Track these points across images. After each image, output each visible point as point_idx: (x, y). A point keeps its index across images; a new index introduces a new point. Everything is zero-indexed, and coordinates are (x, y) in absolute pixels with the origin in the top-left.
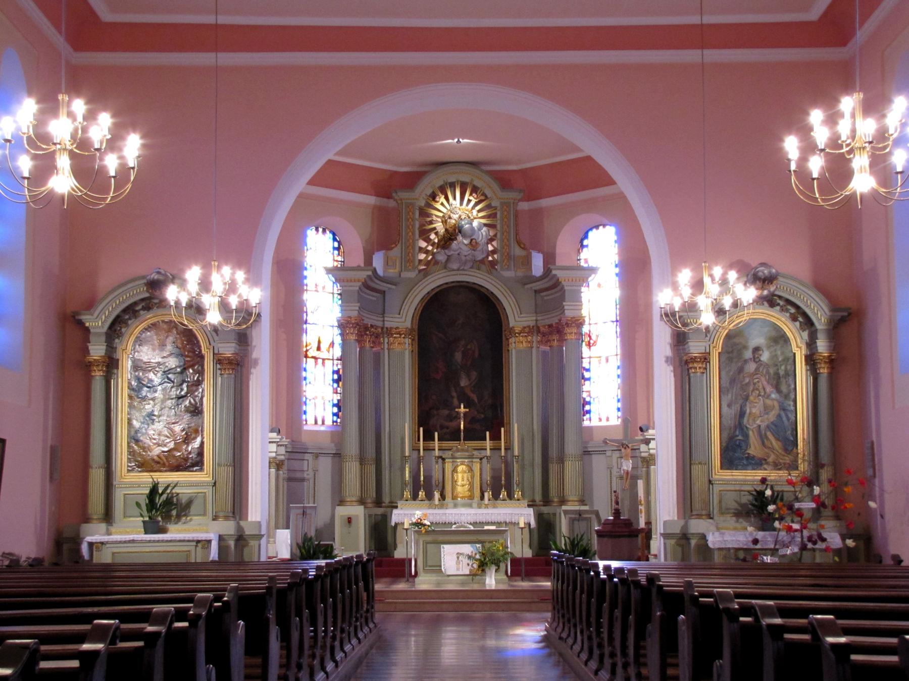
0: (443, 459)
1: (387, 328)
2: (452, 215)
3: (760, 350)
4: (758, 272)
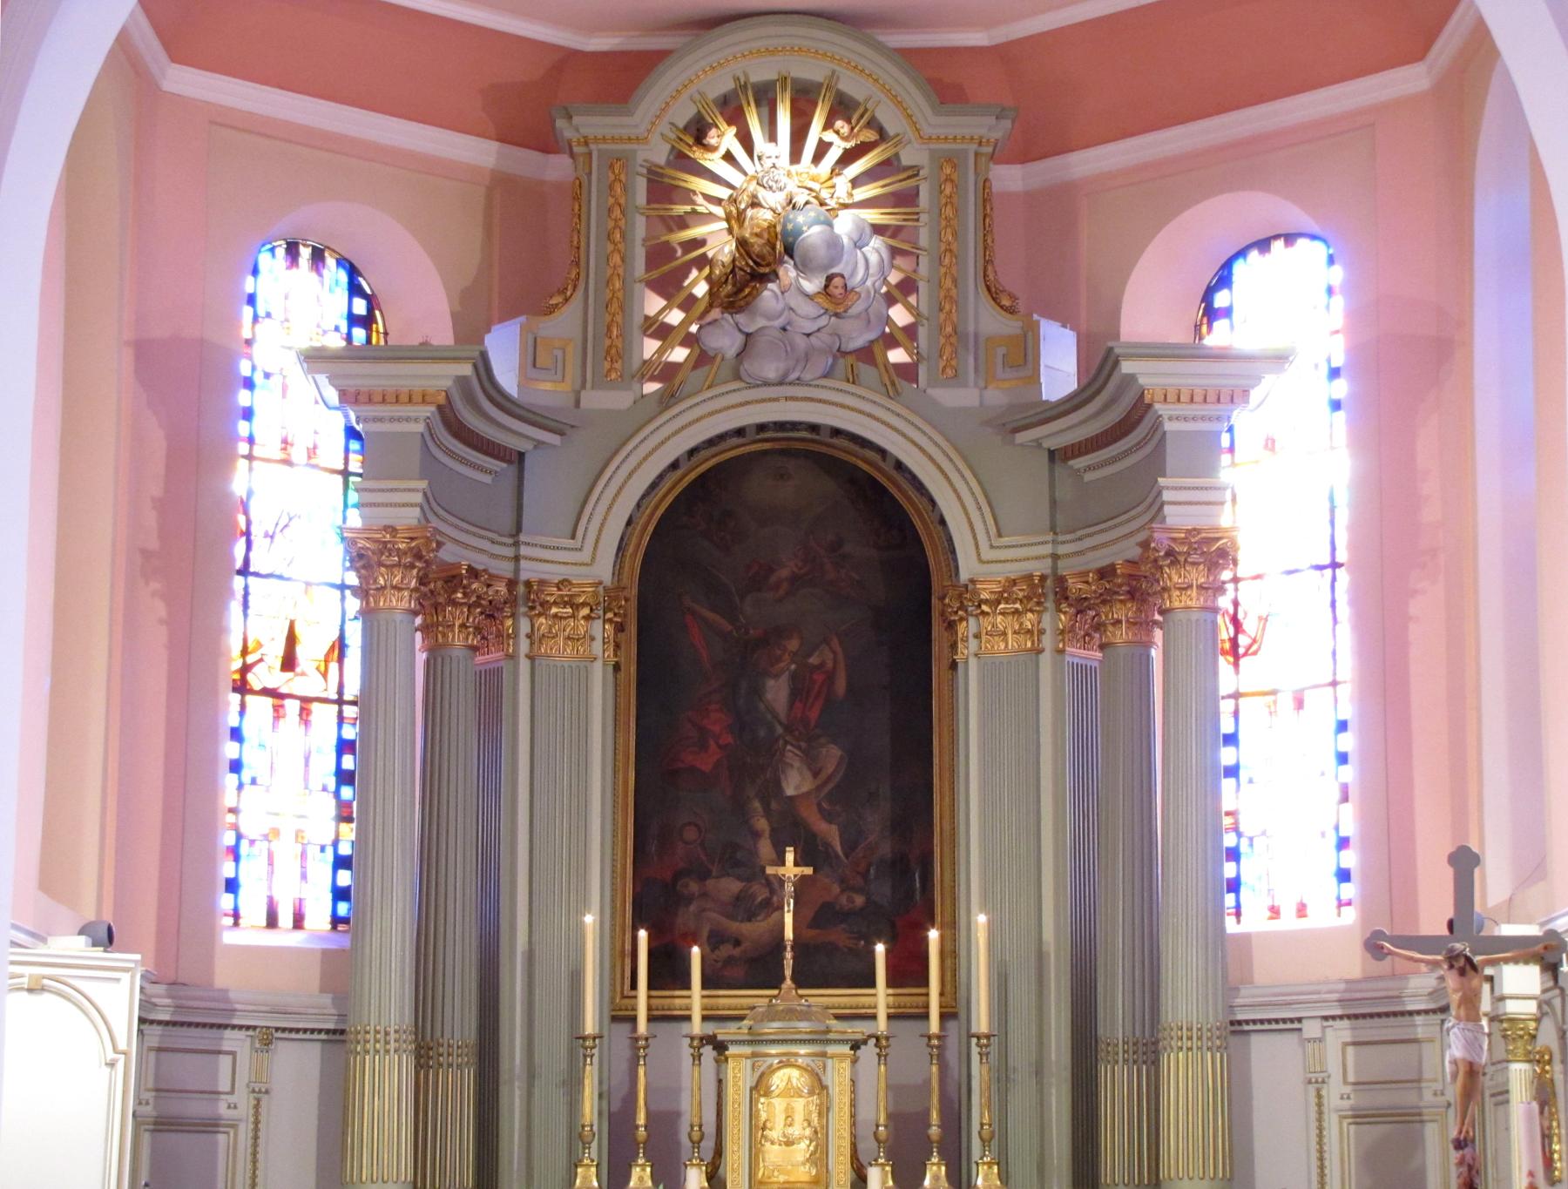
0: (720, 1047)
1: (528, 584)
2: (763, 194)
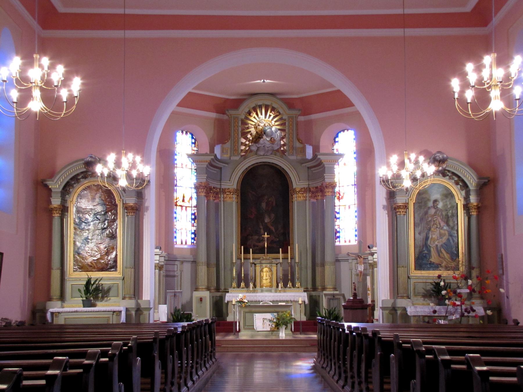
0: (255, 264)
1: (223, 189)
2: (260, 124)
3: (437, 202)
4: (436, 156)
